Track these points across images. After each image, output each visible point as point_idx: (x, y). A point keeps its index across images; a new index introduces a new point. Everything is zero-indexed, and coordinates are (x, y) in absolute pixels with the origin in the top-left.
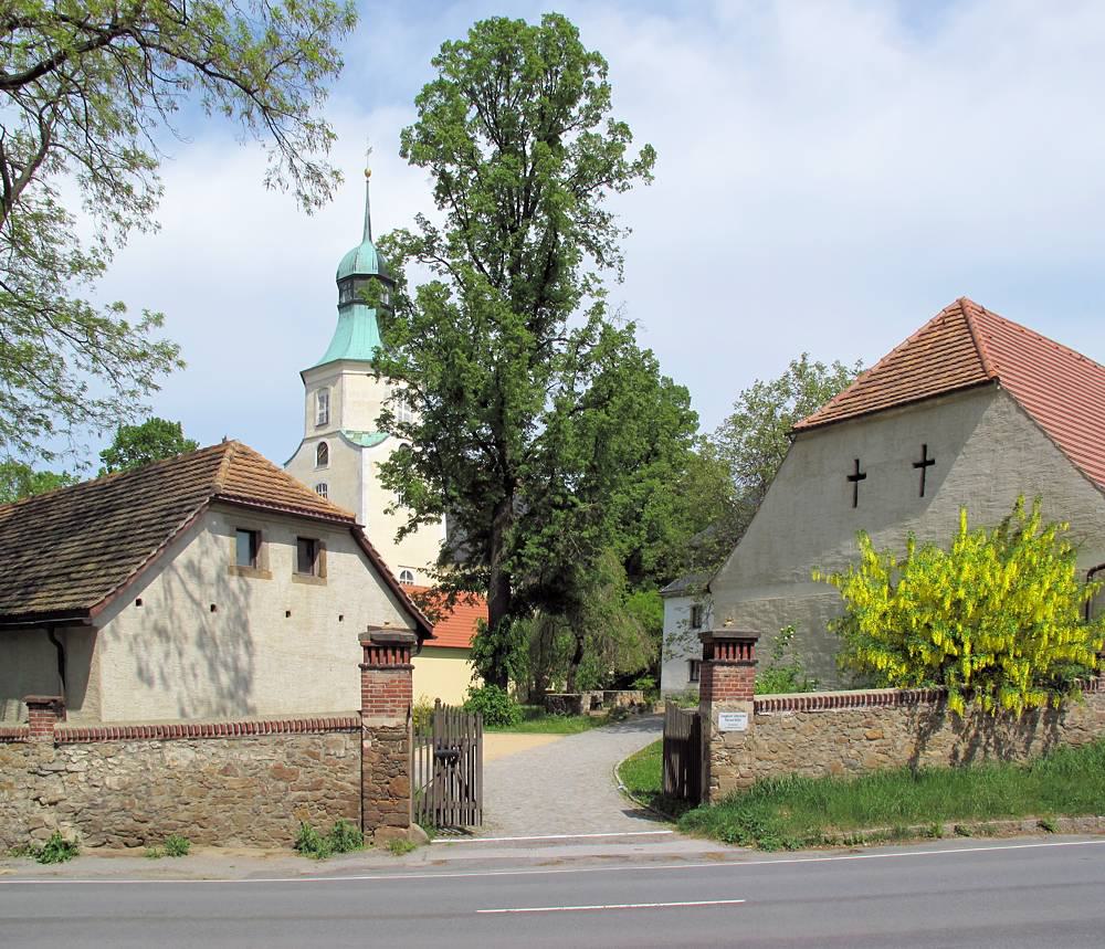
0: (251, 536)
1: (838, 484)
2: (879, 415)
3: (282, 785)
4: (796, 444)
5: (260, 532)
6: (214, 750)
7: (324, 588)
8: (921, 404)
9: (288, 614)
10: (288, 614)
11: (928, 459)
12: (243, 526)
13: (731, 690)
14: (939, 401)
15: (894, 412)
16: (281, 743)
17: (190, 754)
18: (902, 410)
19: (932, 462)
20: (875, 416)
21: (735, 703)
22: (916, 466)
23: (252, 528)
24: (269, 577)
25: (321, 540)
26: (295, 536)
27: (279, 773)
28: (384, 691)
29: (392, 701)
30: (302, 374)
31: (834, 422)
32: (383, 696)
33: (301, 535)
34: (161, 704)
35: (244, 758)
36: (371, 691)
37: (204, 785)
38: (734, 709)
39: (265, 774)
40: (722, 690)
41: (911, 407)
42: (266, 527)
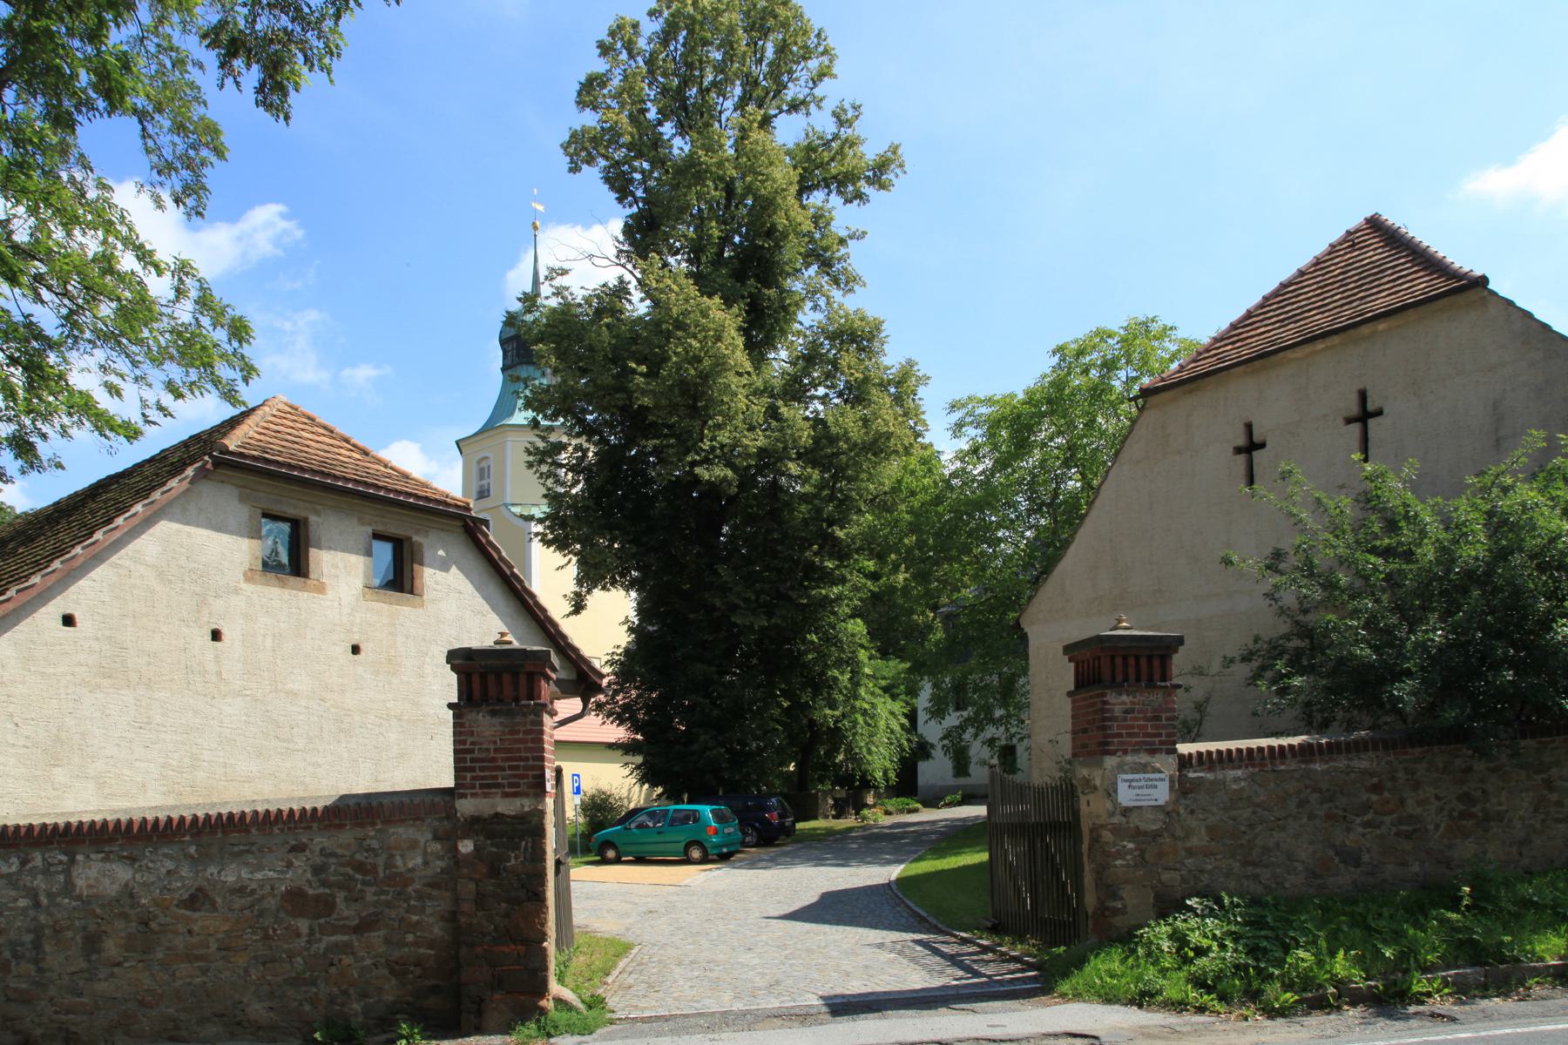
0: (292, 528)
1: (1220, 461)
2: (1281, 355)
3: (303, 925)
4: (1146, 413)
5: (306, 520)
6: (170, 865)
7: (420, 610)
8: (1351, 332)
9: (356, 650)
10: (356, 650)
11: (1370, 407)
12: (276, 508)
13: (1136, 735)
14: (1382, 326)
15: (1308, 349)
16: (299, 849)
17: (123, 873)
18: (1320, 345)
19: (1379, 413)
20: (1274, 358)
21: (1144, 758)
22: (1349, 421)
23: (291, 512)
24: (321, 589)
25: (415, 538)
26: (370, 530)
27: (295, 900)
28: (496, 750)
29: (511, 768)
30: (457, 443)
31: (1208, 374)
32: (493, 760)
33: (380, 528)
34: (107, 791)
35: (230, 878)
36: (472, 751)
37: (145, 934)
38: (1144, 768)
39: (272, 903)
40: (1120, 735)
41: (1336, 339)
42: (317, 513)
